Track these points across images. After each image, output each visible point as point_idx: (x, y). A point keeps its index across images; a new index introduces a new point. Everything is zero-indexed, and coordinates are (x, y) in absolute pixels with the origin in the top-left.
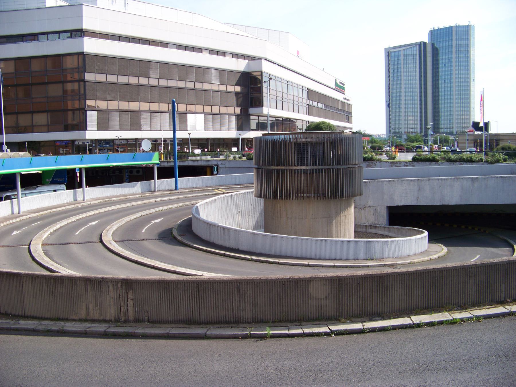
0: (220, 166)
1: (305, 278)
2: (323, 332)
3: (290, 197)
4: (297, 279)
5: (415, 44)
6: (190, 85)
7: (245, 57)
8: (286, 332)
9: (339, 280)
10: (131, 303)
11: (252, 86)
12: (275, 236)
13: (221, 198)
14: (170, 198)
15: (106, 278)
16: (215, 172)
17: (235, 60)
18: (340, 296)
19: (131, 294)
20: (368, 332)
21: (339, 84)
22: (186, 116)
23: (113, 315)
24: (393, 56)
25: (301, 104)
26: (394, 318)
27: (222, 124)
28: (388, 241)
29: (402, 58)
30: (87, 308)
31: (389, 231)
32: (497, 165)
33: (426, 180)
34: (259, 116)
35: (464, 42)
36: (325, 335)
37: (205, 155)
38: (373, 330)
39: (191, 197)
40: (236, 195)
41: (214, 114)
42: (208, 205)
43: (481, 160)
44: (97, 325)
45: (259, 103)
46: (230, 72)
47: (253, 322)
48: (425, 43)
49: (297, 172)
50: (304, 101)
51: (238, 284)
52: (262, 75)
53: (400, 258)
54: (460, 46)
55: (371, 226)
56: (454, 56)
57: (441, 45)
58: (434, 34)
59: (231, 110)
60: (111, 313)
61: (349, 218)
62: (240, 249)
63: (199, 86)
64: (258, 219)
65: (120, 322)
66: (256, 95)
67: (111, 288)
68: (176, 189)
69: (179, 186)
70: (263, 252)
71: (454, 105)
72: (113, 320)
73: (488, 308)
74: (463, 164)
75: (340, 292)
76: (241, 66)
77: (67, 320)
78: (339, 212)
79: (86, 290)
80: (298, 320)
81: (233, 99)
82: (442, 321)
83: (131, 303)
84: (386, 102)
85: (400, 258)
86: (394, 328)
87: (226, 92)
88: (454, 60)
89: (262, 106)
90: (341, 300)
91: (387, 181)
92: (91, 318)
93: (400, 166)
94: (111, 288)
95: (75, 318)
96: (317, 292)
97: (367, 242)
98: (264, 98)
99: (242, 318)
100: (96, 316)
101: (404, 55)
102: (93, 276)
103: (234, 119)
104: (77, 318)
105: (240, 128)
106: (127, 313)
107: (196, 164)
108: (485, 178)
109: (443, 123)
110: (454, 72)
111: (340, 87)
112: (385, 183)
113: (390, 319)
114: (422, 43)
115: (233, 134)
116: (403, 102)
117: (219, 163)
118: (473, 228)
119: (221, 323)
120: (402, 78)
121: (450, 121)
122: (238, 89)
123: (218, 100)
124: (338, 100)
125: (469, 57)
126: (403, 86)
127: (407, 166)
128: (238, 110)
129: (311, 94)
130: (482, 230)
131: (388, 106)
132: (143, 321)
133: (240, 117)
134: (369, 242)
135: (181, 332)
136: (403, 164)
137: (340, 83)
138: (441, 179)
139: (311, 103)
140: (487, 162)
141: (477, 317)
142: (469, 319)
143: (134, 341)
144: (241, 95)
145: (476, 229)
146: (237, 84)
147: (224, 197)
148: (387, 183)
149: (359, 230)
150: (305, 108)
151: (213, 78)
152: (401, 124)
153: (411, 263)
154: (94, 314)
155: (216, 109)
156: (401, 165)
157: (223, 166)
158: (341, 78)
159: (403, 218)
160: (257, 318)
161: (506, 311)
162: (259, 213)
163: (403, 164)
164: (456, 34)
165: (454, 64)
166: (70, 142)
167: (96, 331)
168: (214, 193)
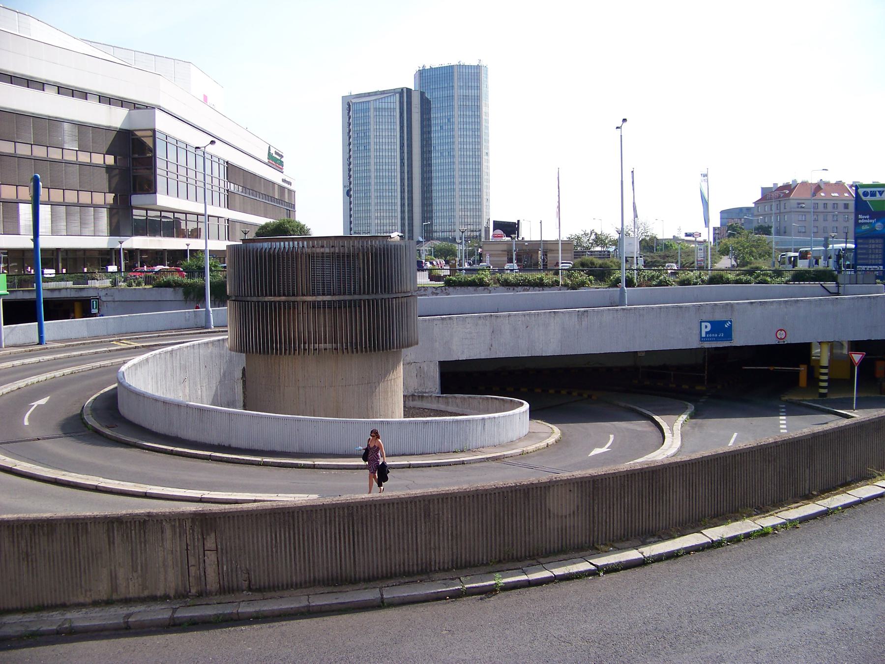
0: (104, 299)
1: (539, 483)
2: (586, 571)
3: (295, 350)
4: (528, 485)
5: (393, 92)
6: (23, 150)
7: (122, 102)
8: (524, 577)
9: (593, 481)
10: (211, 557)
11: (136, 156)
12: (299, 420)
13: (155, 355)
14: (41, 358)
15: (157, 515)
16: (94, 311)
17: (104, 107)
18: (596, 509)
19: (213, 540)
20: (653, 562)
21: (274, 155)
22: (18, 207)
23: (173, 585)
24: (356, 111)
25: (216, 189)
26: (679, 536)
27: (83, 223)
28: (483, 419)
29: (372, 113)
30: (113, 578)
31: (447, 404)
32: (581, 290)
33: (505, 316)
34: (147, 210)
35: (471, 92)
36: (589, 575)
37: (62, 280)
38: (659, 558)
39: (79, 356)
40: (179, 349)
41: (68, 205)
42: (136, 369)
43: (557, 283)
44: (141, 608)
45: (150, 187)
46: (96, 128)
47: (453, 568)
48: (409, 91)
49: (315, 305)
50: (222, 183)
51: (427, 502)
52: (154, 137)
53: (501, 445)
54: (466, 97)
55: (413, 395)
56: (456, 113)
57: (436, 94)
58: (424, 75)
59: (99, 198)
60: (168, 580)
61: (397, 384)
62: (234, 445)
63: (40, 152)
64: (217, 390)
65: (188, 597)
66: (143, 172)
67: (168, 533)
68: (41, 342)
69: (46, 336)
70: (278, 448)
71: (457, 193)
72: (172, 595)
73: (797, 507)
74: (528, 290)
75: (596, 502)
76: (115, 118)
77: (64, 607)
78: (387, 373)
79: (111, 542)
80: (530, 556)
81: (103, 179)
82: (748, 533)
83: (211, 557)
84: (344, 187)
85: (501, 445)
86: (688, 551)
87: (90, 165)
88: (456, 120)
89: (155, 193)
90: (596, 515)
91: (438, 319)
92: (122, 596)
93: (425, 295)
94: (168, 533)
95: (81, 600)
96: (561, 505)
97: (453, 421)
98: (159, 178)
99: (433, 563)
100: (133, 591)
101: (375, 109)
102: (124, 512)
103: (104, 214)
104: (88, 600)
105: (115, 231)
106: (203, 578)
107: (56, 295)
108: (598, 312)
109: (439, 224)
110: (457, 140)
111: (275, 160)
112: (435, 322)
113: (674, 538)
114: (405, 90)
115: (102, 242)
116: (373, 188)
117: (102, 294)
118: (569, 393)
119: (396, 576)
120: (372, 147)
121: (451, 221)
122: (110, 160)
123: (75, 181)
124: (274, 183)
125: (479, 117)
126: (372, 161)
127: (437, 294)
128: (110, 197)
129: (232, 171)
130: (585, 396)
131: (348, 193)
132: (239, 590)
133: (115, 211)
134: (457, 421)
135: (335, 601)
136: (430, 291)
137: (276, 153)
138: (530, 315)
139: (232, 187)
140: (566, 285)
141: (791, 521)
142: (784, 525)
143: (245, 630)
144: (117, 171)
145: (575, 394)
146: (108, 153)
147: (160, 354)
148: (439, 322)
149: (411, 404)
150: (222, 196)
151: (67, 138)
152: (369, 225)
153: (522, 454)
154: (127, 587)
155: (71, 197)
156: (426, 293)
157: (110, 299)
158: (279, 146)
159: (469, 380)
160: (459, 560)
161: (823, 508)
162: (218, 380)
163: (430, 291)
164: (459, 79)
165: (456, 127)
166: (82, 252)
167: (151, 620)
168: (119, 348)
